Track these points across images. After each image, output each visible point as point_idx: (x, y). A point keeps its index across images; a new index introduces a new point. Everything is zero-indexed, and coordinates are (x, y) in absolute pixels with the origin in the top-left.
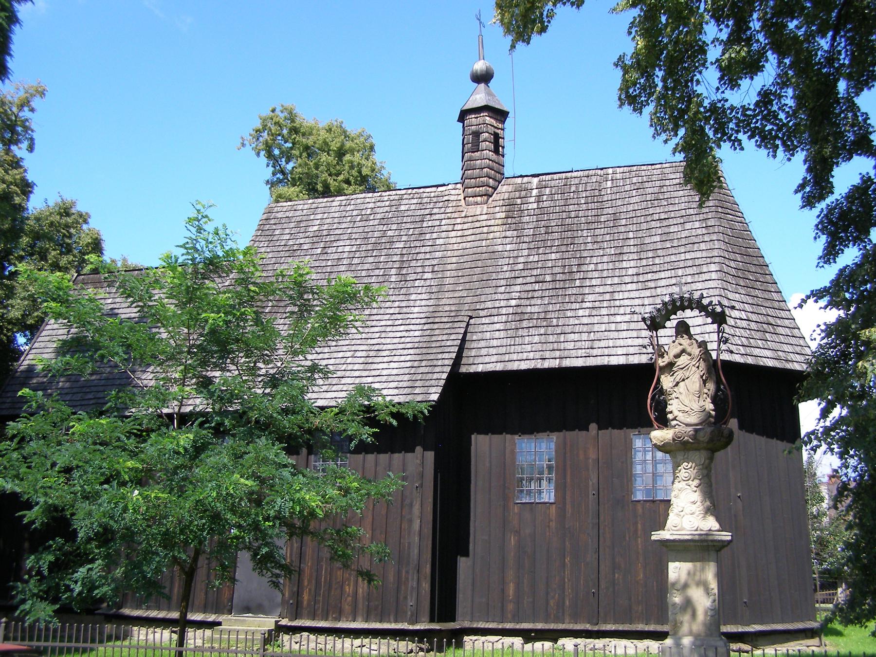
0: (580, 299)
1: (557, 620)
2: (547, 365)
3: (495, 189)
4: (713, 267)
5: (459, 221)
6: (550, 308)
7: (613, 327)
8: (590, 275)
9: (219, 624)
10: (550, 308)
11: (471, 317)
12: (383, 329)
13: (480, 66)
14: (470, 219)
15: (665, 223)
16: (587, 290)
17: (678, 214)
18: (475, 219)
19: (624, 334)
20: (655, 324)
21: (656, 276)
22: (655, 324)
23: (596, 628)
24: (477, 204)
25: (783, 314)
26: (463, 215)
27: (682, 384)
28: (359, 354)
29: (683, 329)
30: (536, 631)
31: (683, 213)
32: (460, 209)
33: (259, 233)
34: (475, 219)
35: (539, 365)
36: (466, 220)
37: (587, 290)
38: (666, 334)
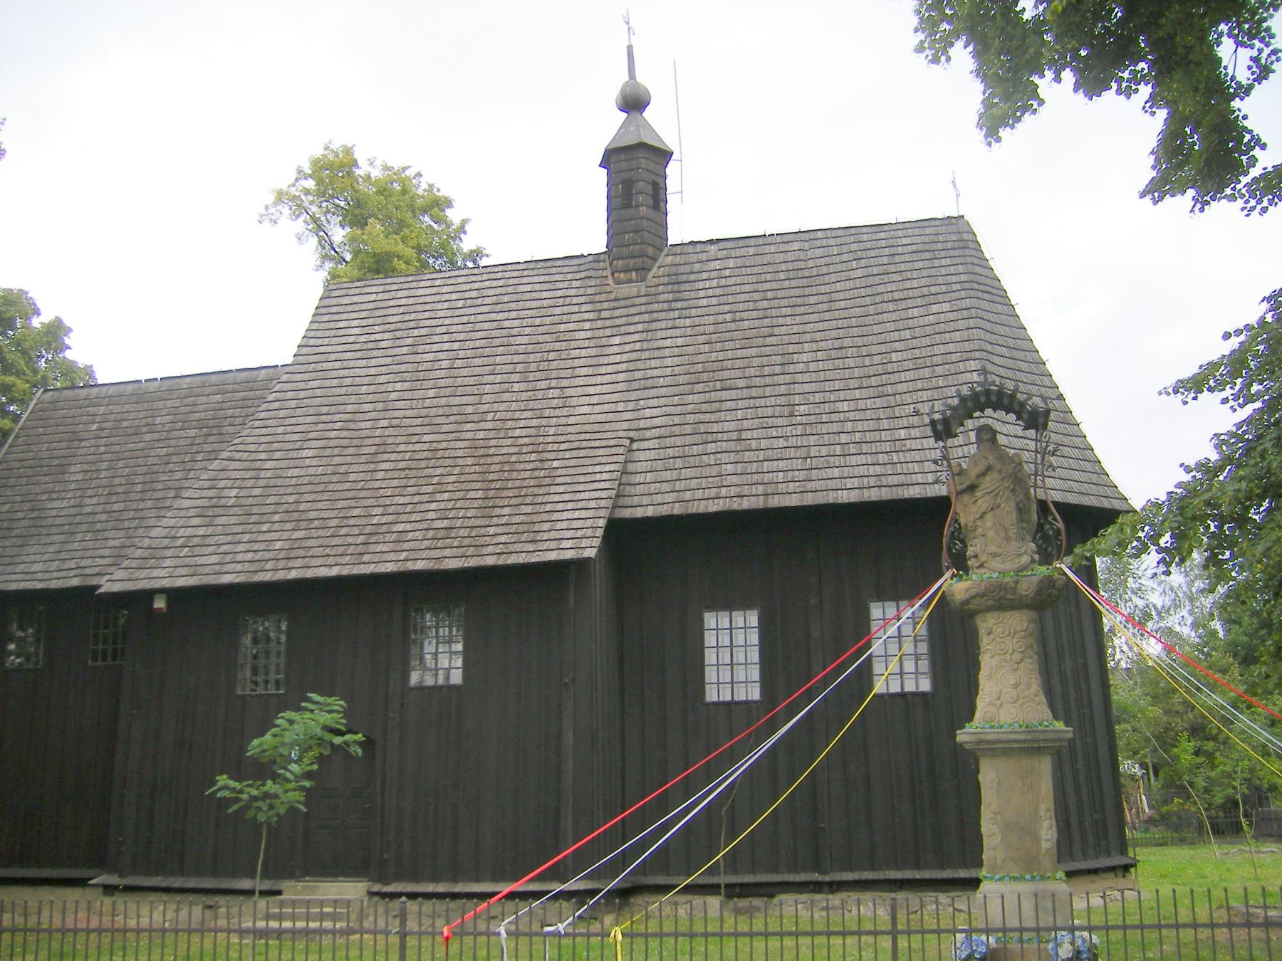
0: (786, 411)
1: (776, 870)
2: (746, 504)
3: (655, 260)
4: (973, 365)
5: (606, 305)
6: (746, 424)
7: (838, 449)
8: (799, 378)
9: (279, 893)
10: (746, 424)
11: (632, 440)
12: (506, 458)
13: (378, 285)
14: (622, 303)
15: (903, 305)
16: (797, 399)
17: (916, 293)
18: (629, 302)
19: (854, 460)
20: (943, 430)
21: (894, 378)
22: (943, 430)
23: (827, 878)
24: (630, 281)
25: (1069, 429)
26: (612, 296)
27: (989, 516)
28: (471, 495)
29: (987, 436)
30: (742, 885)
31: (925, 291)
32: (608, 289)
33: (315, 326)
34: (629, 302)
35: (736, 505)
36: (616, 304)
37: (797, 399)
38: (964, 446)
